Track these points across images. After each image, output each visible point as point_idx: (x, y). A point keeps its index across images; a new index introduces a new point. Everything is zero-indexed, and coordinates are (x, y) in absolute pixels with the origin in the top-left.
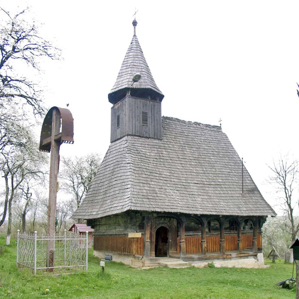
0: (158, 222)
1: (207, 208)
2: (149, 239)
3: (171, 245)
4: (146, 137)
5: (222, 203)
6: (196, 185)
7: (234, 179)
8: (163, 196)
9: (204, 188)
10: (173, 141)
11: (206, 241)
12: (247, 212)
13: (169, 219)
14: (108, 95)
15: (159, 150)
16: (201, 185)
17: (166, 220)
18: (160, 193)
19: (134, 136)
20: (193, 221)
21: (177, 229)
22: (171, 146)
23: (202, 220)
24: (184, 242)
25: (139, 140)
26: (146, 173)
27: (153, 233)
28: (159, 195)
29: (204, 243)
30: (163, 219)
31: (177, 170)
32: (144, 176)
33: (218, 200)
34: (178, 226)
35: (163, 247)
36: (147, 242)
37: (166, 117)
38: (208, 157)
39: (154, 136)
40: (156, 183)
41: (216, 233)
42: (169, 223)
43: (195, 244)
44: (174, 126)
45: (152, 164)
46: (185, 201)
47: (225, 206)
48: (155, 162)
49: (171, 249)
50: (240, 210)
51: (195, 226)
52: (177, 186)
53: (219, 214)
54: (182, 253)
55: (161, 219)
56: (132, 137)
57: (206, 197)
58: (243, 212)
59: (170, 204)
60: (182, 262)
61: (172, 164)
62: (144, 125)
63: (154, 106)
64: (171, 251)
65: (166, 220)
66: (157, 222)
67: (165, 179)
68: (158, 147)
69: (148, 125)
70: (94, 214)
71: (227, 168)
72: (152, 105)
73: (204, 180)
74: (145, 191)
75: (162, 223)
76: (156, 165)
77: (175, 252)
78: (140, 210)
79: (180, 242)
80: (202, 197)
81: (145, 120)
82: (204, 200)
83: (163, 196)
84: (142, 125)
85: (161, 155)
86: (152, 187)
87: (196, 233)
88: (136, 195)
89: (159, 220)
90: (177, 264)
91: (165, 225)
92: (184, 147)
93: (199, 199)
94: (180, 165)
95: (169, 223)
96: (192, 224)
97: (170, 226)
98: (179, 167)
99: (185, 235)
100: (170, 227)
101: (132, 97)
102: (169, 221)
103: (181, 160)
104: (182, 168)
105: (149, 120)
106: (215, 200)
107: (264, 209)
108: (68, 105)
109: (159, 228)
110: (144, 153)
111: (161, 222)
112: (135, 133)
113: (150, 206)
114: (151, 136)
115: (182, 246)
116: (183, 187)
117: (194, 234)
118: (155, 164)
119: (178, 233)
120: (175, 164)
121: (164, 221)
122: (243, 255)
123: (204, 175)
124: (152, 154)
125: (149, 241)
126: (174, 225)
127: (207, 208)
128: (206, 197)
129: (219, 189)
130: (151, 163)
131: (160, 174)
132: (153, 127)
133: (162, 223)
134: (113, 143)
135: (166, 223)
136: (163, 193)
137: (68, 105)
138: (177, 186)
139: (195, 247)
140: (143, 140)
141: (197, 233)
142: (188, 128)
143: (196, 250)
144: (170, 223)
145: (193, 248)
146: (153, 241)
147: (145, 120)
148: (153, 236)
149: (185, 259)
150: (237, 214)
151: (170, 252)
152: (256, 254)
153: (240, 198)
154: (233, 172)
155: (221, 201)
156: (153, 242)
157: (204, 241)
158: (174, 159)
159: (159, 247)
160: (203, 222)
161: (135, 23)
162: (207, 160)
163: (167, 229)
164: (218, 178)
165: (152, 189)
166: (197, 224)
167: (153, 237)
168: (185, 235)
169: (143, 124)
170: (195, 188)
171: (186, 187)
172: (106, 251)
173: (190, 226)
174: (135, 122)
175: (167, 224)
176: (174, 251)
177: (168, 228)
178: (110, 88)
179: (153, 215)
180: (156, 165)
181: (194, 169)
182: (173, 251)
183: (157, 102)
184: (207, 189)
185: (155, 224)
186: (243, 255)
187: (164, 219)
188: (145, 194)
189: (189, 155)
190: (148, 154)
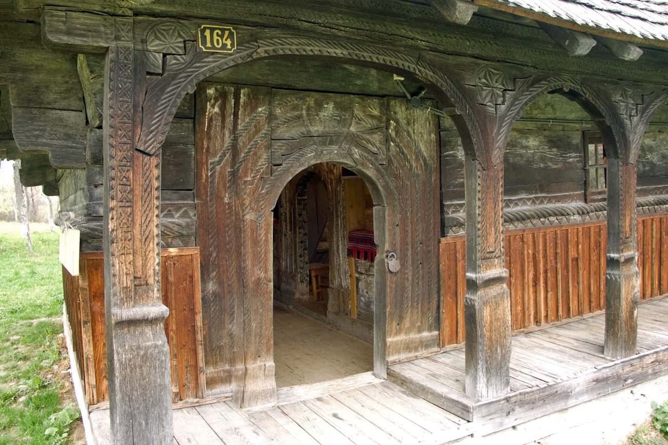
0: (294, 132)
2: (156, 293)
3: (401, 290)
13: (376, 113)
17: (358, 112)
20: (531, 125)
21: (434, 178)
23: (613, 110)
24: (497, 280)
27: (250, 216)
29: (624, 270)
30: (329, 109)
34: (443, 164)
35: (358, 280)
36: (132, 323)
41: (651, 198)
42: (377, 138)
43: (546, 272)
49: (401, 318)
51: (543, 159)
54: (488, 371)
55: (319, 106)
64: (398, 332)
65: (358, 112)
66: (284, 132)
75: (327, 139)
77: (426, 334)
79: (472, 285)
87: (550, 200)
89: (299, 117)
91: (351, 155)
95: (377, 138)
96: (527, 147)
97: (390, 162)
99: (509, 220)
100: (387, 168)
102: (382, 124)
108: (632, 392)
109: (297, 175)
111: (317, 129)
115: (485, 315)
117: (539, 207)
119: (442, 206)
121: (341, 122)
125: (158, 309)
126: (418, 154)
133: (327, 139)
135: (355, 140)
137: (632, 392)
139: (546, 292)
141: (558, 199)
143: (551, 303)
144: (387, 139)
145: (535, 292)
146: (251, 280)
148: (256, 242)
151: (389, 340)
156: (258, 282)
157: (629, 260)
159: (336, 282)
160: (622, 125)
163: (369, 179)
166: (558, 147)
167: (249, 249)
168: (509, 220)
173: (521, 155)
175: (359, 145)
176: (420, 331)
177: (370, 172)
179: (189, 44)
182: (414, 336)
185: (269, 147)
187: (338, 106)
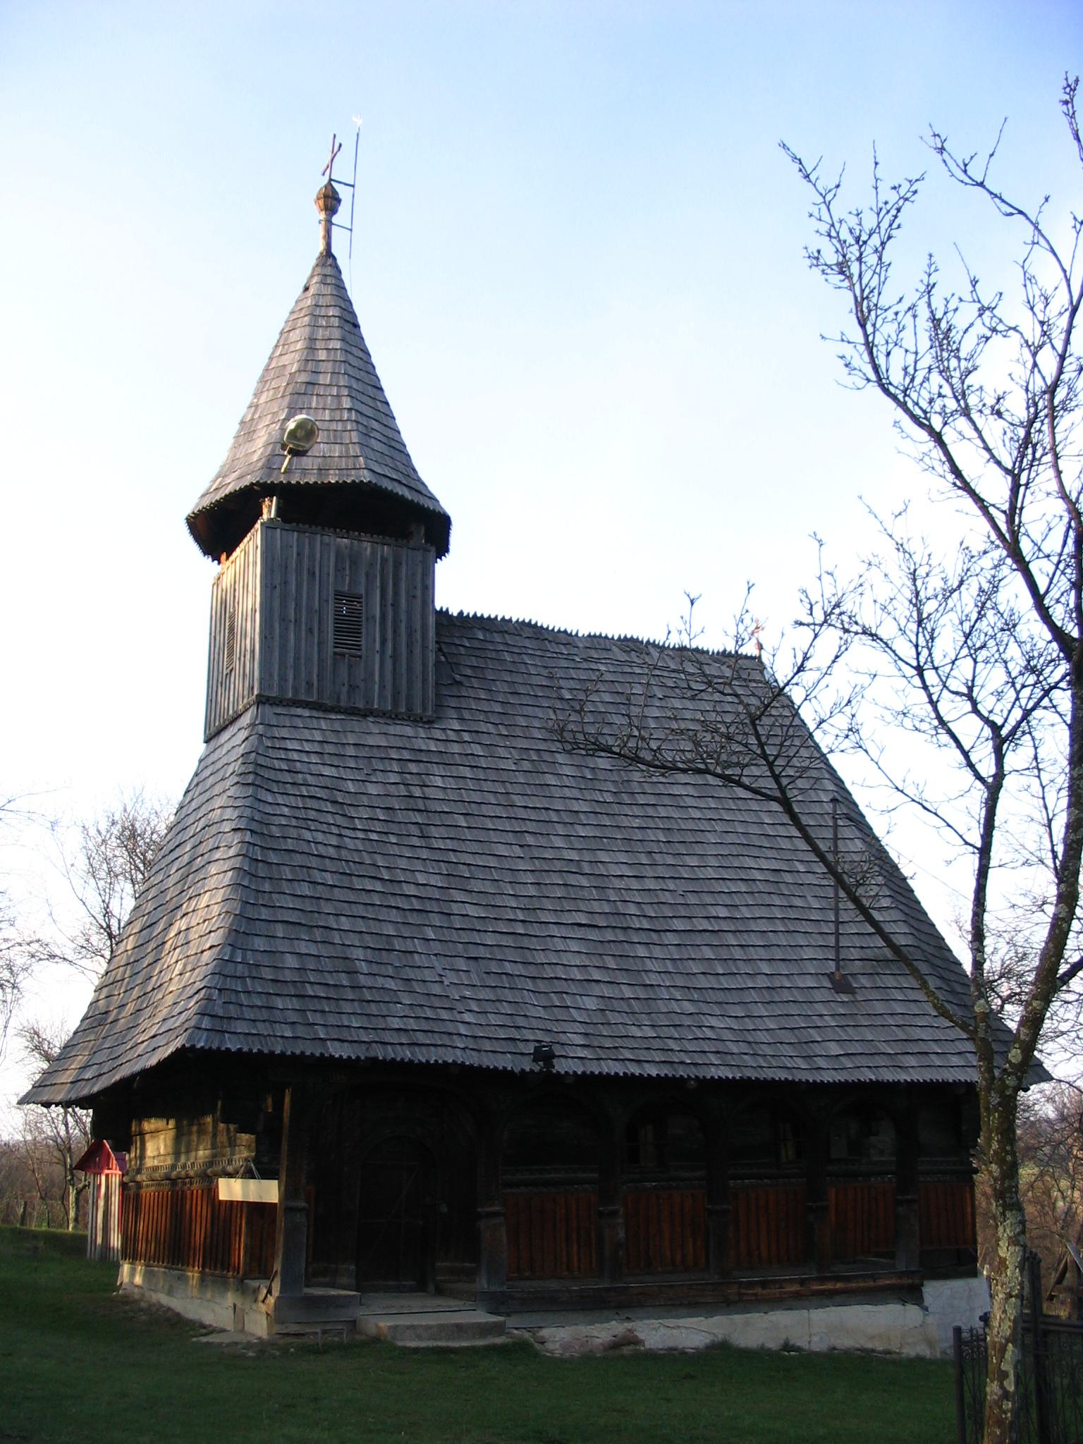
1: (619, 1042)
4: (353, 712)
5: (714, 1022)
6: (580, 933)
7: (798, 902)
8: (391, 984)
9: (628, 950)
10: (491, 728)
11: (622, 1211)
12: (847, 1063)
14: (447, 551)
15: (413, 768)
16: (609, 935)
18: (375, 969)
19: (288, 705)
22: (478, 750)
24: (496, 1214)
25: (315, 724)
26: (318, 877)
28: (363, 980)
31: (492, 862)
32: (305, 889)
33: (690, 1008)
37: (503, 619)
38: (667, 801)
39: (395, 702)
40: (361, 926)
44: (508, 657)
45: (361, 835)
46: (507, 1009)
47: (727, 1035)
48: (378, 827)
50: (807, 1057)
52: (477, 938)
53: (681, 1072)
56: (279, 710)
57: (627, 992)
58: (821, 1063)
59: (412, 1024)
60: (482, 1317)
61: (468, 835)
62: (343, 655)
63: (397, 565)
67: (416, 904)
68: (406, 755)
69: (363, 653)
70: (87, 1078)
71: (770, 854)
72: (384, 560)
73: (632, 909)
74: (291, 961)
76: (384, 838)
78: (303, 1053)
80: (607, 991)
81: (349, 627)
82: (617, 1005)
83: (391, 984)
84: (335, 653)
85: (417, 792)
86: (337, 941)
88: (239, 981)
90: (442, 1327)
92: (546, 757)
93: (591, 1004)
94: (510, 838)
98: (502, 850)
101: (287, 526)
103: (522, 814)
104: (518, 851)
105: (371, 637)
106: (675, 1006)
107: (950, 1048)
110: (329, 783)
112: (296, 690)
113: (301, 1031)
114: (342, 704)
116: (508, 941)
118: (374, 836)
120: (482, 836)
122: (839, 1285)
123: (635, 884)
124: (372, 789)
127: (619, 1042)
128: (627, 992)
129: (708, 953)
130: (354, 829)
131: (391, 881)
132: (389, 662)
134: (213, 743)
136: (390, 971)
138: (477, 938)
140: (337, 726)
142: (585, 665)
147: (349, 627)
149: (497, 1303)
150: (782, 1075)
152: (917, 1281)
153: (818, 995)
154: (801, 868)
155: (705, 1008)
158: (485, 810)
161: (330, 201)
162: (663, 812)
164: (708, 899)
165: (338, 952)
169: (337, 650)
170: (574, 946)
171: (526, 942)
172: (158, 1262)
174: (298, 639)
178: (192, 498)
180: (384, 838)
181: (587, 856)
183: (412, 543)
184: (641, 951)
186: (839, 1285)
188: (288, 976)
189: (568, 793)
190: (351, 787)
